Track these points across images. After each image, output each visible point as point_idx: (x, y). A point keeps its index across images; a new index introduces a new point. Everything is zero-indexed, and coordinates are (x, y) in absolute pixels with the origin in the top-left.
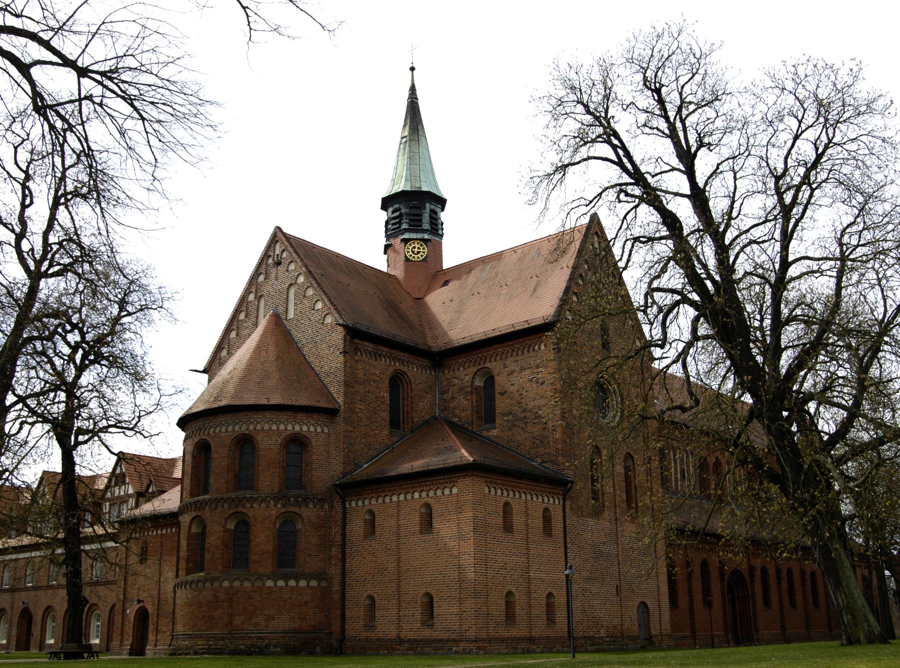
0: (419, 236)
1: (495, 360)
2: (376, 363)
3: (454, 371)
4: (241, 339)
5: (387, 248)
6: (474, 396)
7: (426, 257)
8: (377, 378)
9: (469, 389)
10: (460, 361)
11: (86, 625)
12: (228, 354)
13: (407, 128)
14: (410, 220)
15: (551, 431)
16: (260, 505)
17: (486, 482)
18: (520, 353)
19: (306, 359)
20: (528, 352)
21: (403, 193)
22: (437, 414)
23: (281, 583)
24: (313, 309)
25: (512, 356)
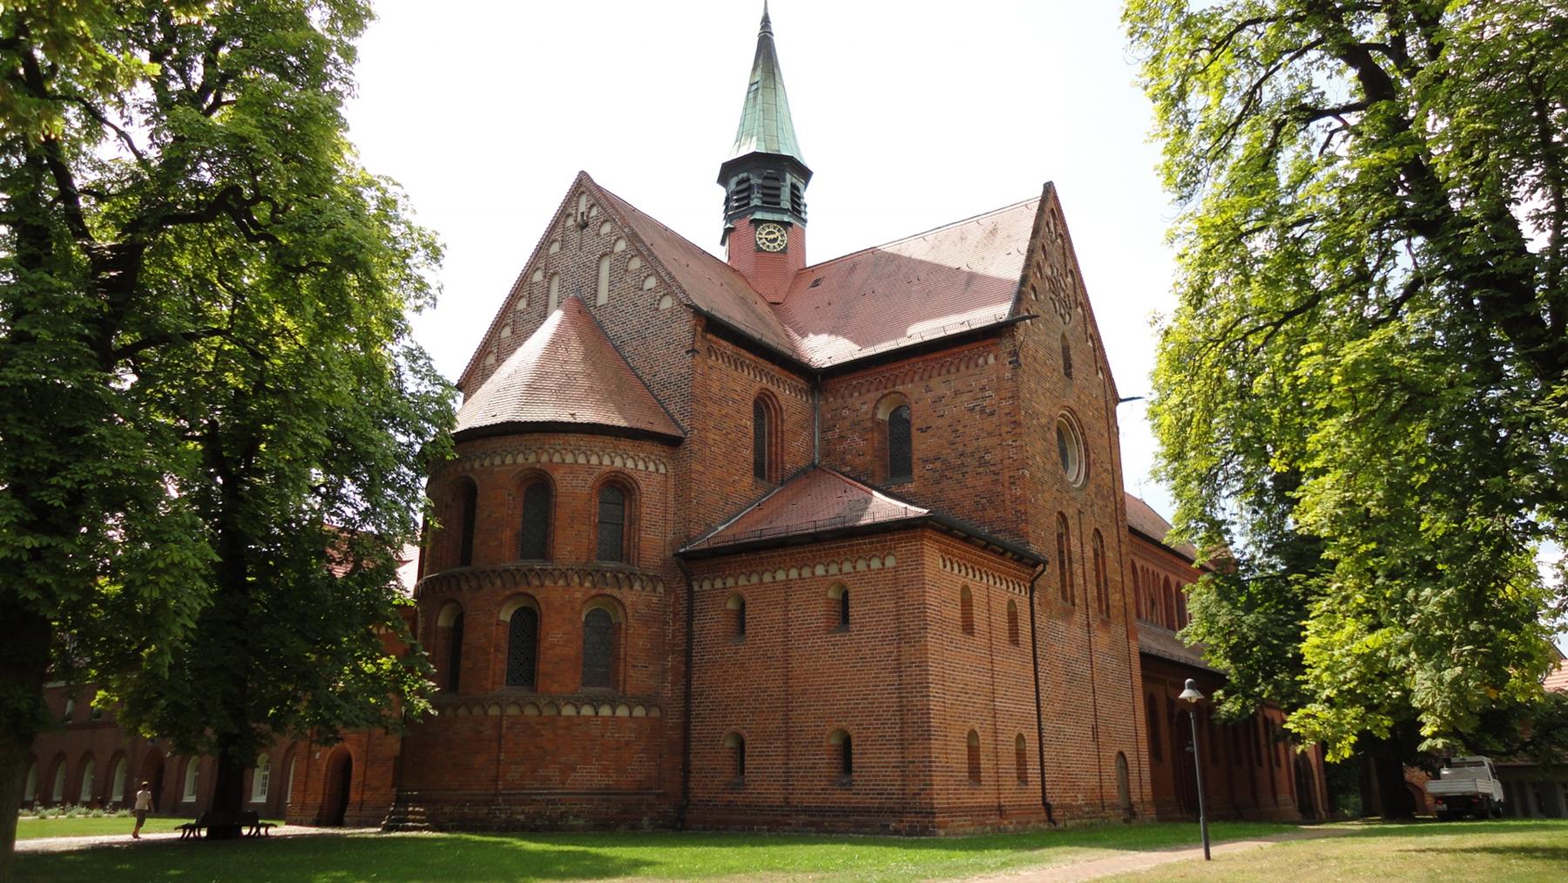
0: (777, 217)
1: (912, 381)
2: (735, 374)
3: (843, 397)
4: (520, 338)
5: (727, 232)
6: (876, 434)
7: (786, 247)
8: (738, 398)
9: (869, 424)
10: (854, 383)
11: (1559, 826)
12: (497, 360)
13: (759, 71)
14: (764, 194)
15: (1007, 484)
16: (556, 583)
17: (940, 550)
18: (953, 369)
19: (628, 364)
20: (967, 367)
21: (754, 156)
22: (817, 461)
23: (587, 711)
24: (641, 289)
25: (939, 375)
